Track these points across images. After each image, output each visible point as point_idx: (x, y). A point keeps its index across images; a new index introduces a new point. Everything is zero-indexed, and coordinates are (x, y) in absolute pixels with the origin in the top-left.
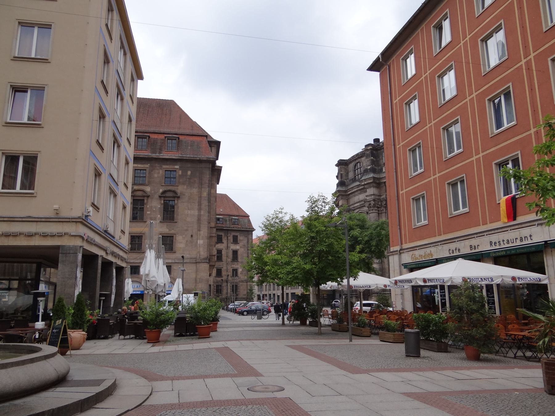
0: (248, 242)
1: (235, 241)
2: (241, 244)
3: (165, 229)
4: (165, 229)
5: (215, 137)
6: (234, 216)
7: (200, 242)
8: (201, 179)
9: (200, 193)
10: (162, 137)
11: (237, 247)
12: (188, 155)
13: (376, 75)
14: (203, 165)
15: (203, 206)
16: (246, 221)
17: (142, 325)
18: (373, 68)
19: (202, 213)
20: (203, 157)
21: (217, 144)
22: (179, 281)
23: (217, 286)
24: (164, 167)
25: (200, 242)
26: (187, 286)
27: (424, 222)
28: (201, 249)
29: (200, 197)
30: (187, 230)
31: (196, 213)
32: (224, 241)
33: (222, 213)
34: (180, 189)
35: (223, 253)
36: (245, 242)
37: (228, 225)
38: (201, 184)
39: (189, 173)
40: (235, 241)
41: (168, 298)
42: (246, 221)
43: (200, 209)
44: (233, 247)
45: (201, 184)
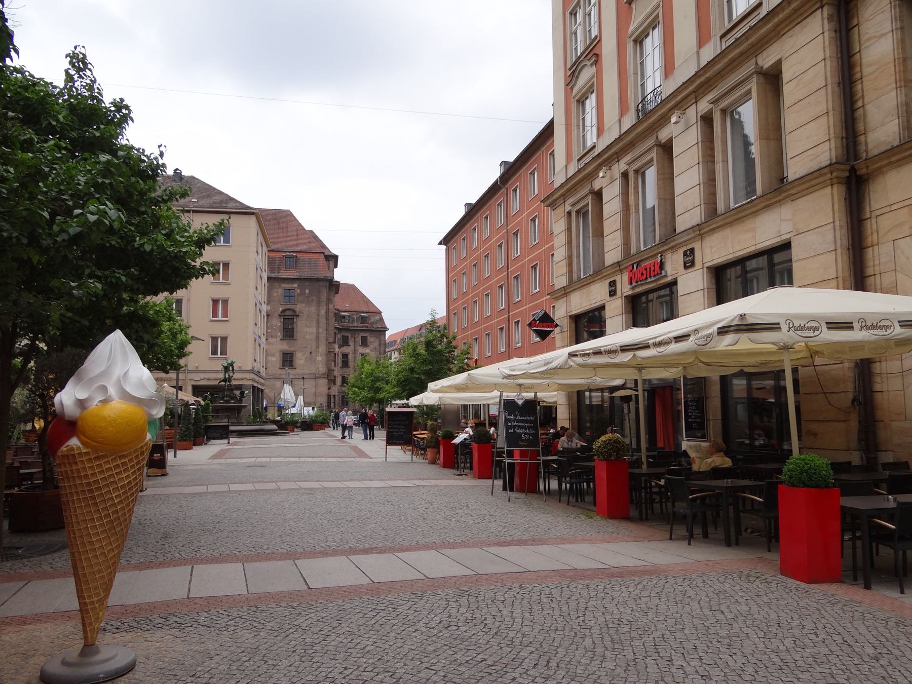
0: (380, 344)
1: (365, 343)
2: (371, 346)
3: (285, 346)
4: (285, 346)
5: (334, 251)
6: (363, 312)
7: (319, 358)
8: (319, 298)
9: (318, 311)
10: (281, 255)
11: (366, 350)
12: (306, 274)
13: (444, 247)
14: (321, 283)
15: (321, 324)
16: (378, 318)
17: (287, 425)
18: (440, 243)
19: (320, 330)
20: (321, 275)
21: (335, 258)
22: (301, 398)
23: (343, 397)
24: (283, 285)
25: (319, 358)
26: (307, 400)
27: (489, 354)
28: (320, 365)
29: (318, 315)
30: (306, 347)
31: (314, 330)
32: (351, 343)
33: (348, 309)
34: (299, 308)
35: (350, 357)
36: (377, 344)
37: (356, 323)
38: (319, 302)
39: (307, 291)
40: (365, 343)
41: (203, 403)
42: (378, 318)
43: (318, 327)
44: (361, 350)
45: (319, 302)
